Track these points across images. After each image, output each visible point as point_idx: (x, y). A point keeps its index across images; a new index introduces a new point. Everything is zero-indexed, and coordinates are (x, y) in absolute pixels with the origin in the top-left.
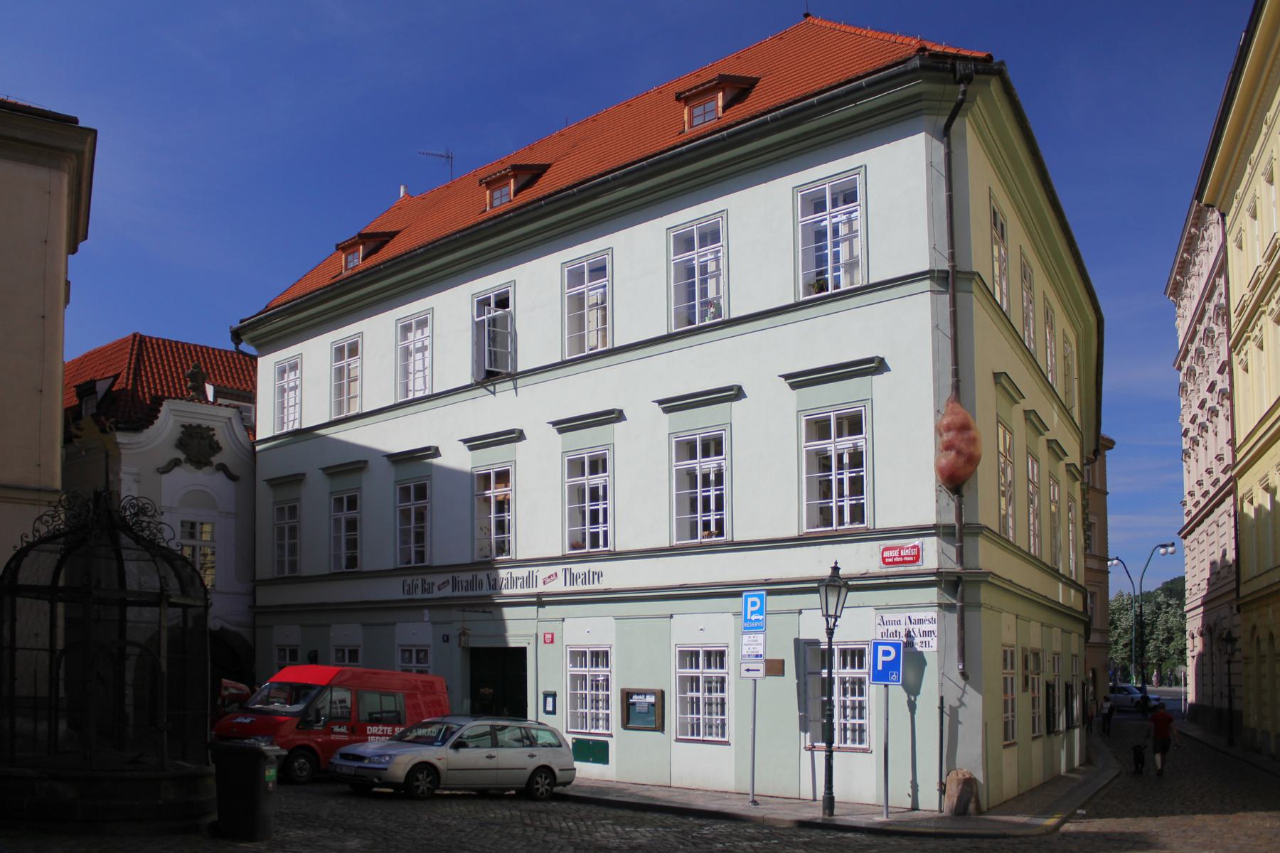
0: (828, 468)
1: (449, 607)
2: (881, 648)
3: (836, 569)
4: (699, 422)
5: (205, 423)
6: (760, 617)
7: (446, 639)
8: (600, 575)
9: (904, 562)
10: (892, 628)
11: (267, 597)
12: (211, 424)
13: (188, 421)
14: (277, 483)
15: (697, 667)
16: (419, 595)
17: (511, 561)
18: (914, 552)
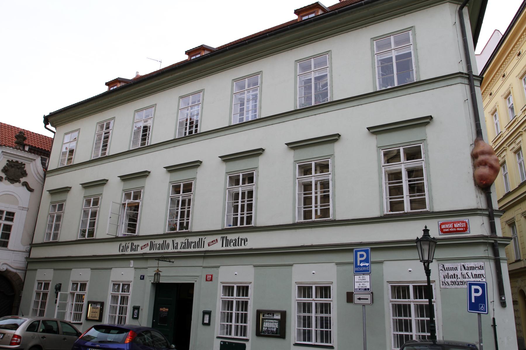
1: (147, 259)
2: (473, 287)
3: (426, 231)
4: (182, 177)
5: (20, 161)
6: (367, 264)
7: (142, 278)
8: (246, 240)
9: (457, 232)
10: (451, 273)
11: (37, 253)
12: (24, 162)
13: (11, 159)
14: (53, 192)
15: (232, 295)
16: (129, 252)
18: (464, 225)
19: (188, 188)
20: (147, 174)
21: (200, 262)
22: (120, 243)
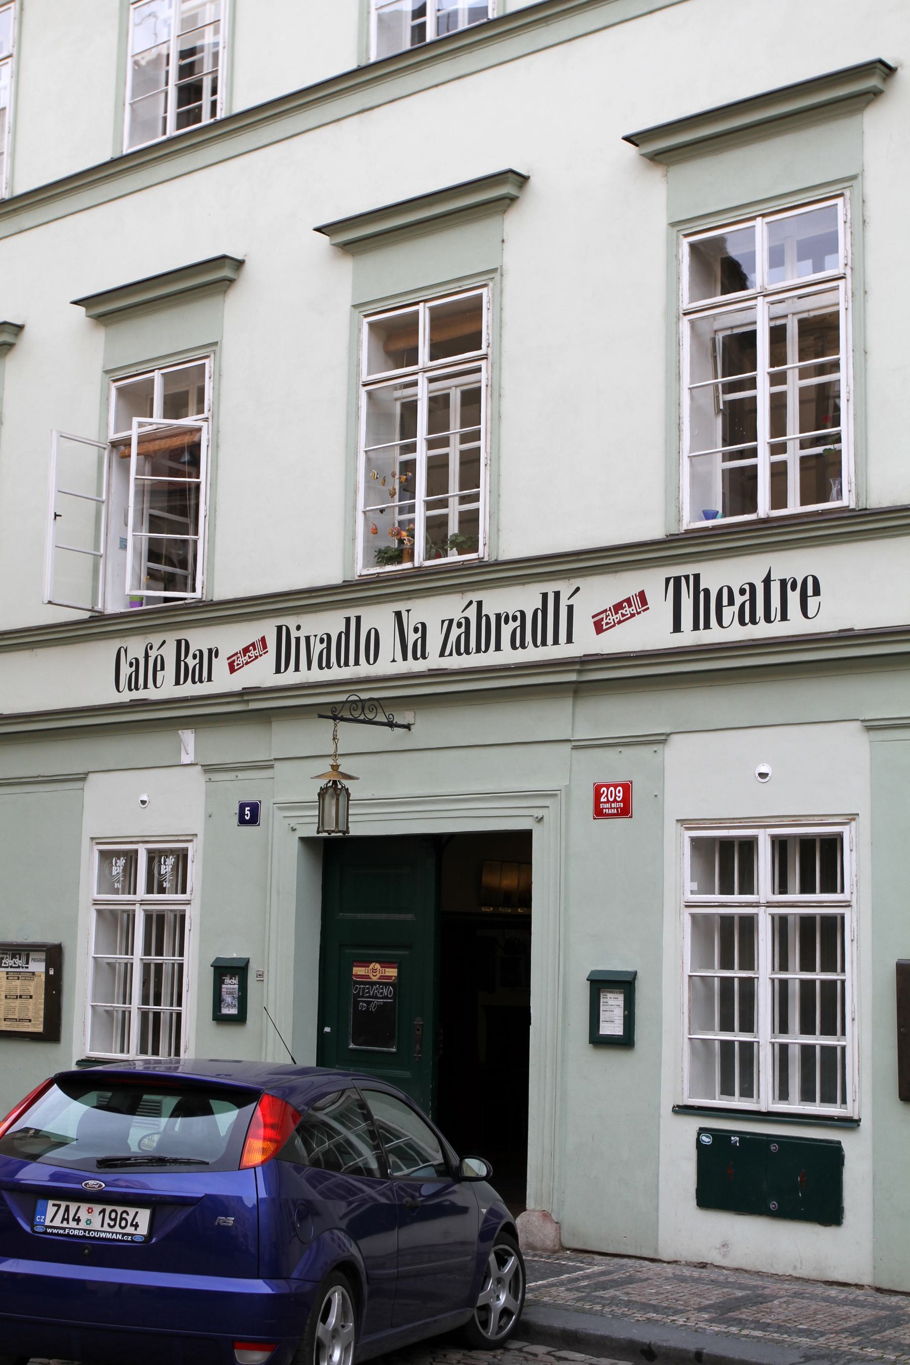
0: (408, 428)
1: (265, 717)
7: (249, 815)
8: (810, 589)
16: (166, 687)
17: (482, 565)
19: (459, 328)
20: (226, 273)
21: (556, 719)
22: (113, 646)
